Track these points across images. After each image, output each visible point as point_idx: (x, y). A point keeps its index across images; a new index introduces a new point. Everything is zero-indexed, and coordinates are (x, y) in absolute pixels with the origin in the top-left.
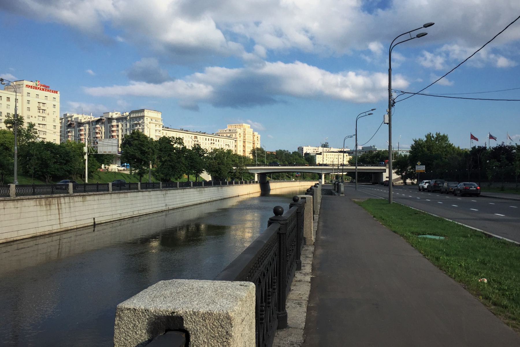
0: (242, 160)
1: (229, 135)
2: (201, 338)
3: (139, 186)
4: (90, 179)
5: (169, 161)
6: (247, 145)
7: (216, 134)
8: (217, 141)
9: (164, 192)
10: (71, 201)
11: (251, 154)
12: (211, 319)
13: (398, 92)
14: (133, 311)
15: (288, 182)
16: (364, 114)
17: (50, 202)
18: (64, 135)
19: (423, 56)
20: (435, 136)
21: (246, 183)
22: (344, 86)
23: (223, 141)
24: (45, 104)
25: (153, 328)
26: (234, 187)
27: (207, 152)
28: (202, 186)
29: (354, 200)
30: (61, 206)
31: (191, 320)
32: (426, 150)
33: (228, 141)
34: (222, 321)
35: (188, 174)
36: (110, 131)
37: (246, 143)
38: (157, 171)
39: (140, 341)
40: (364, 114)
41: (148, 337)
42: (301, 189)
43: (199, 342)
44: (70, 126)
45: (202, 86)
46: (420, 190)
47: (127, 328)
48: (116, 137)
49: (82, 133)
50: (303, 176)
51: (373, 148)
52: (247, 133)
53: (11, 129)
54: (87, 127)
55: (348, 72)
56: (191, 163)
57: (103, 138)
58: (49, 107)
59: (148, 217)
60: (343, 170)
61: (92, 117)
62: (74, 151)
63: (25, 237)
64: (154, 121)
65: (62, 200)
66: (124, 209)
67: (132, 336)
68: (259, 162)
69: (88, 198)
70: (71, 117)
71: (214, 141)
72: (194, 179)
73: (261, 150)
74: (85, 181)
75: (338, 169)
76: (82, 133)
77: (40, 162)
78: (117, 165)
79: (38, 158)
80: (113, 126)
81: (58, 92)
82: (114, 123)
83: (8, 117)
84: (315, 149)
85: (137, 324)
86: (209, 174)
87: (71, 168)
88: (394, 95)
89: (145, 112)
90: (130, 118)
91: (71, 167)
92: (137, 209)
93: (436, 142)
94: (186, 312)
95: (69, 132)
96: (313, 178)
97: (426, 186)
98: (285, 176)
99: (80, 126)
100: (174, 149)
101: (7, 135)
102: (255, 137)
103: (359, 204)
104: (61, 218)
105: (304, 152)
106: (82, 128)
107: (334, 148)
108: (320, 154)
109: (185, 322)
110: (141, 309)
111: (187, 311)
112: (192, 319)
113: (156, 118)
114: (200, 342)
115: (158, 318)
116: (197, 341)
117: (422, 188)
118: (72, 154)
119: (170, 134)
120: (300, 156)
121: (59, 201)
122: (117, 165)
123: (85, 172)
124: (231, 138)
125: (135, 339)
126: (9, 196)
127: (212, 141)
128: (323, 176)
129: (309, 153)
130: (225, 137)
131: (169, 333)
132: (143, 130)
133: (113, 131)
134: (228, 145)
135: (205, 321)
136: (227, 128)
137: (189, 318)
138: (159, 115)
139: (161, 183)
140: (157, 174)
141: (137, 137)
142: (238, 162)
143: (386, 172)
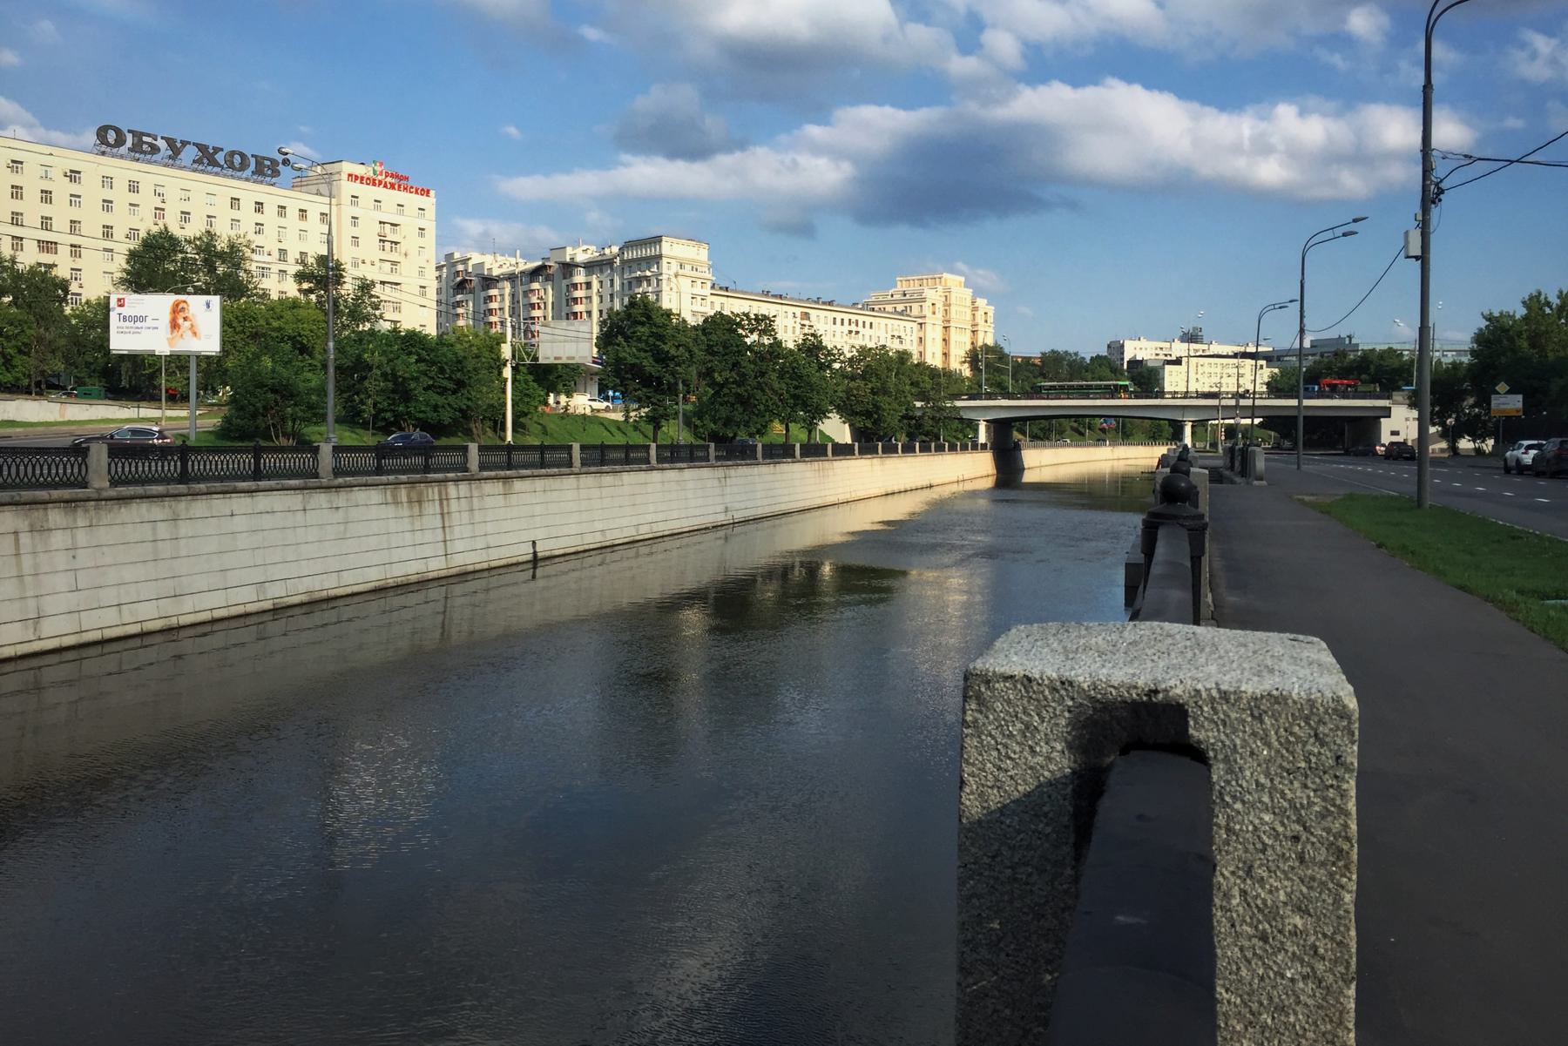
0: (936, 381)
1: (900, 308)
2: (1248, 773)
3: (653, 452)
4: (519, 436)
5: (733, 383)
6: (954, 336)
7: (863, 305)
8: (868, 325)
9: (720, 472)
10: (475, 493)
11: (967, 365)
12: (1283, 716)
13: (1454, 157)
14: (1022, 684)
15: (1077, 446)
16: (1329, 235)
17: (420, 494)
18: (447, 310)
19: (1523, 45)
20: (1555, 301)
21: (953, 448)
22: (1262, 148)
23: (883, 326)
24: (396, 225)
25: (1087, 736)
26: (918, 459)
27: (842, 358)
28: (827, 456)
29: (1300, 497)
30: (448, 505)
31: (1215, 717)
32: (1525, 344)
33: (898, 326)
34: (1321, 722)
35: (786, 422)
36: (567, 300)
37: (952, 330)
38: (699, 414)
39: (1046, 774)
40: (1329, 235)
41: (1072, 765)
42: (1116, 470)
43: (1241, 786)
44: (461, 286)
45: (822, 163)
46: (1508, 470)
47: (1004, 735)
48: (585, 315)
49: (494, 305)
50: (1124, 430)
51: (1347, 342)
52: (953, 301)
53: (313, 297)
54: (507, 287)
55: (1275, 104)
56: (796, 388)
57: (550, 319)
58: (407, 234)
59: (677, 543)
60: (1252, 411)
61: (520, 260)
62: (477, 357)
63: (356, 589)
65: (452, 490)
67: (1019, 758)
68: (991, 386)
69: (518, 485)
70: (465, 261)
71: (857, 325)
72: (803, 436)
73: (996, 352)
74: (504, 439)
75: (1237, 406)
76: (494, 305)
77: (390, 385)
78: (588, 396)
79: (384, 375)
80: (575, 286)
81: (432, 193)
82: (580, 277)
83: (303, 263)
84: (1161, 349)
85: (1035, 724)
86: (844, 423)
87: (470, 403)
88: (1440, 170)
89: (664, 243)
90: (623, 261)
91: (469, 399)
92: (649, 518)
93: (1560, 320)
94: (1198, 691)
95: (458, 304)
96: (1153, 437)
97: (1528, 458)
98: (1068, 429)
99: (489, 288)
100: (750, 348)
101: (302, 313)
102: (980, 315)
103: (1325, 511)
104: (448, 538)
105: (1127, 357)
106: (493, 292)
107: (1220, 343)
108: (1178, 362)
109: (1192, 723)
110: (1049, 679)
111: (1200, 686)
112: (1216, 713)
113: (694, 260)
114: (1245, 784)
115: (1104, 708)
116: (1234, 783)
117: (1514, 464)
118: (470, 364)
119: (733, 306)
120: (1116, 371)
121: (444, 493)
122: (588, 396)
123: (504, 415)
124: (908, 315)
125: (1031, 768)
126: (316, 476)
127: (853, 328)
128: (1188, 430)
129: (1142, 361)
130: (889, 313)
131: (1135, 755)
132: (657, 295)
133: (575, 300)
134: (899, 337)
135: (1262, 722)
136: (895, 286)
137: (1206, 709)
138: (700, 253)
139: (712, 445)
140: (698, 422)
141: (642, 315)
142: (929, 386)
143: (1389, 417)
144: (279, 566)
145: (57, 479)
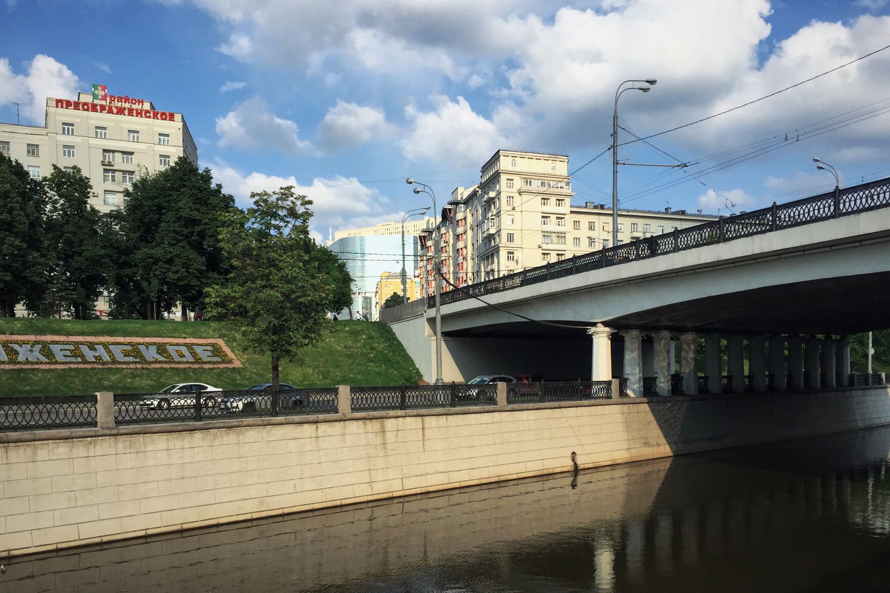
64: (536, 185)
66: (268, 483)
81: (178, 117)
126: (94, 424)
144: (97, 522)
145: (440, 403)
